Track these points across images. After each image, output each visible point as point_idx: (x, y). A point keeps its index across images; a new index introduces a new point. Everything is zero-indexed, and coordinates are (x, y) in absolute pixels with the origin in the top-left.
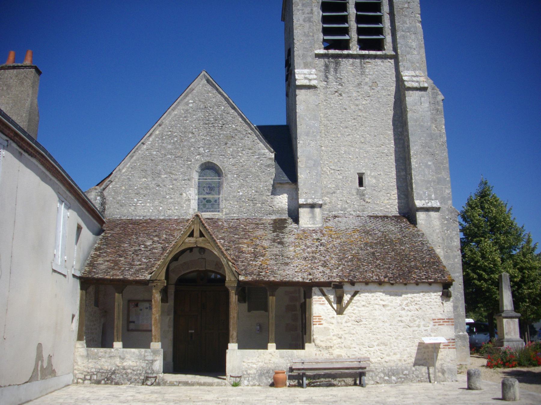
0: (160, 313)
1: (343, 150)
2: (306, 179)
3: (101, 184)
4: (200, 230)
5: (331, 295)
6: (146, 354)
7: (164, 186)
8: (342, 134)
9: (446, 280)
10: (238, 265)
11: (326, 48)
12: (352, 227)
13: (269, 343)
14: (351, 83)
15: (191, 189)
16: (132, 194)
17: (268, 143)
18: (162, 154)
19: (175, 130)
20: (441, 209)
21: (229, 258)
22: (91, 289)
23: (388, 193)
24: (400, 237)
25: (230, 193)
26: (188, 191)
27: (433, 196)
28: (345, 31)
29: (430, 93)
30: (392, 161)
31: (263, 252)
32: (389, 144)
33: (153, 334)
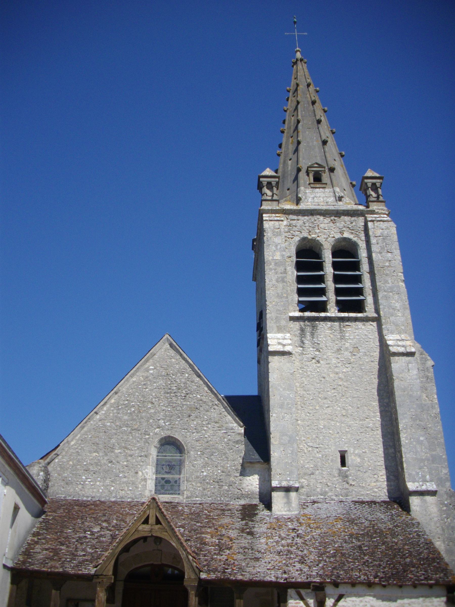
1: (322, 424)
2: (280, 457)
3: (45, 458)
5: (311, 599)
7: (118, 462)
8: (321, 406)
9: (450, 581)
10: (199, 559)
11: (302, 310)
12: (334, 515)
14: (329, 348)
15: (148, 466)
16: (81, 470)
18: (117, 426)
20: (438, 493)
21: (189, 550)
23: (375, 474)
24: (391, 526)
25: (192, 472)
27: (428, 477)
28: (322, 292)
29: (418, 358)
30: (378, 436)
31: (229, 544)
32: (374, 417)
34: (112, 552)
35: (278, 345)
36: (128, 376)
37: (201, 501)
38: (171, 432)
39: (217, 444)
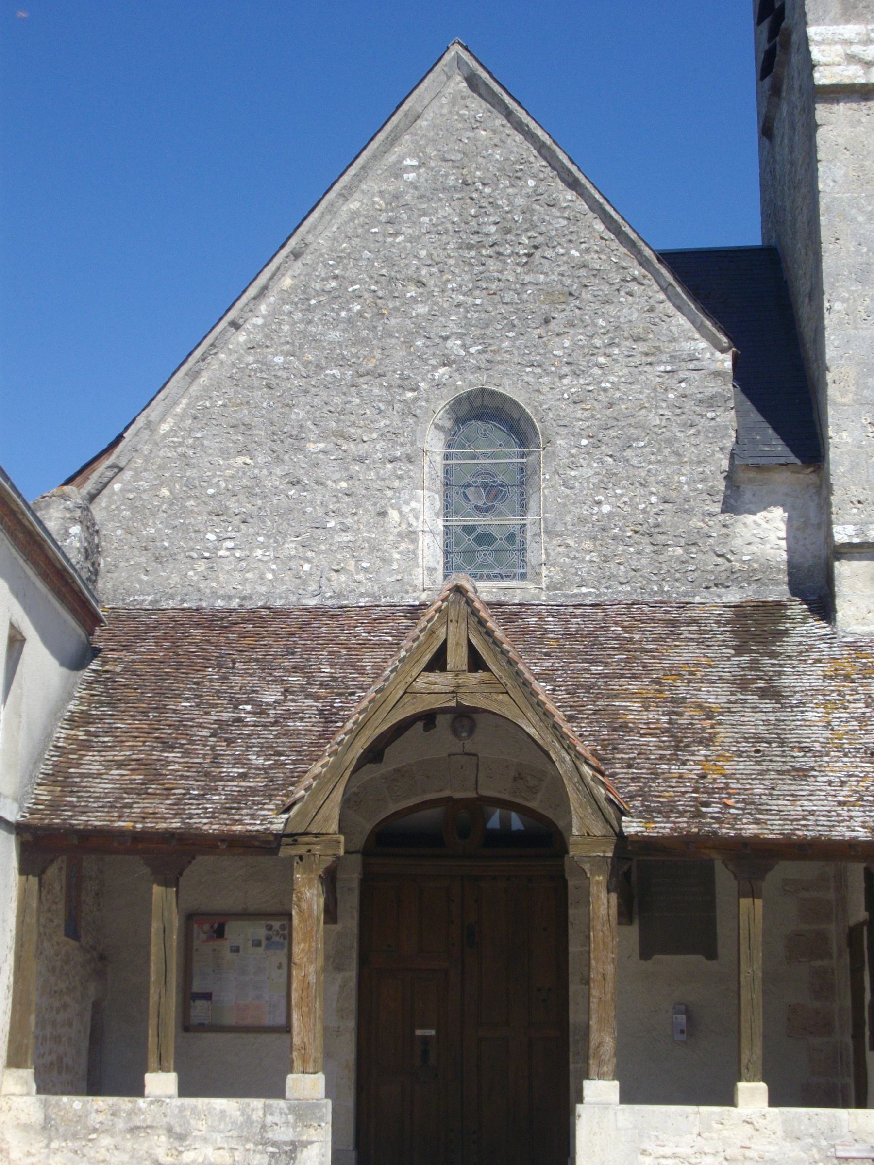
0: (320, 962)
2: (861, 447)
3: (79, 479)
4: (470, 644)
6: (269, 1119)
7: (317, 483)
10: (613, 775)
13: (740, 1081)
15: (420, 492)
17: (707, 315)
18: (306, 364)
19: (351, 273)
22: (56, 873)
26: (407, 503)
33: (296, 1040)
34: (333, 762)
35: (849, 64)
36: (331, 195)
37: (597, 596)
38: (489, 376)
39: (643, 412)
